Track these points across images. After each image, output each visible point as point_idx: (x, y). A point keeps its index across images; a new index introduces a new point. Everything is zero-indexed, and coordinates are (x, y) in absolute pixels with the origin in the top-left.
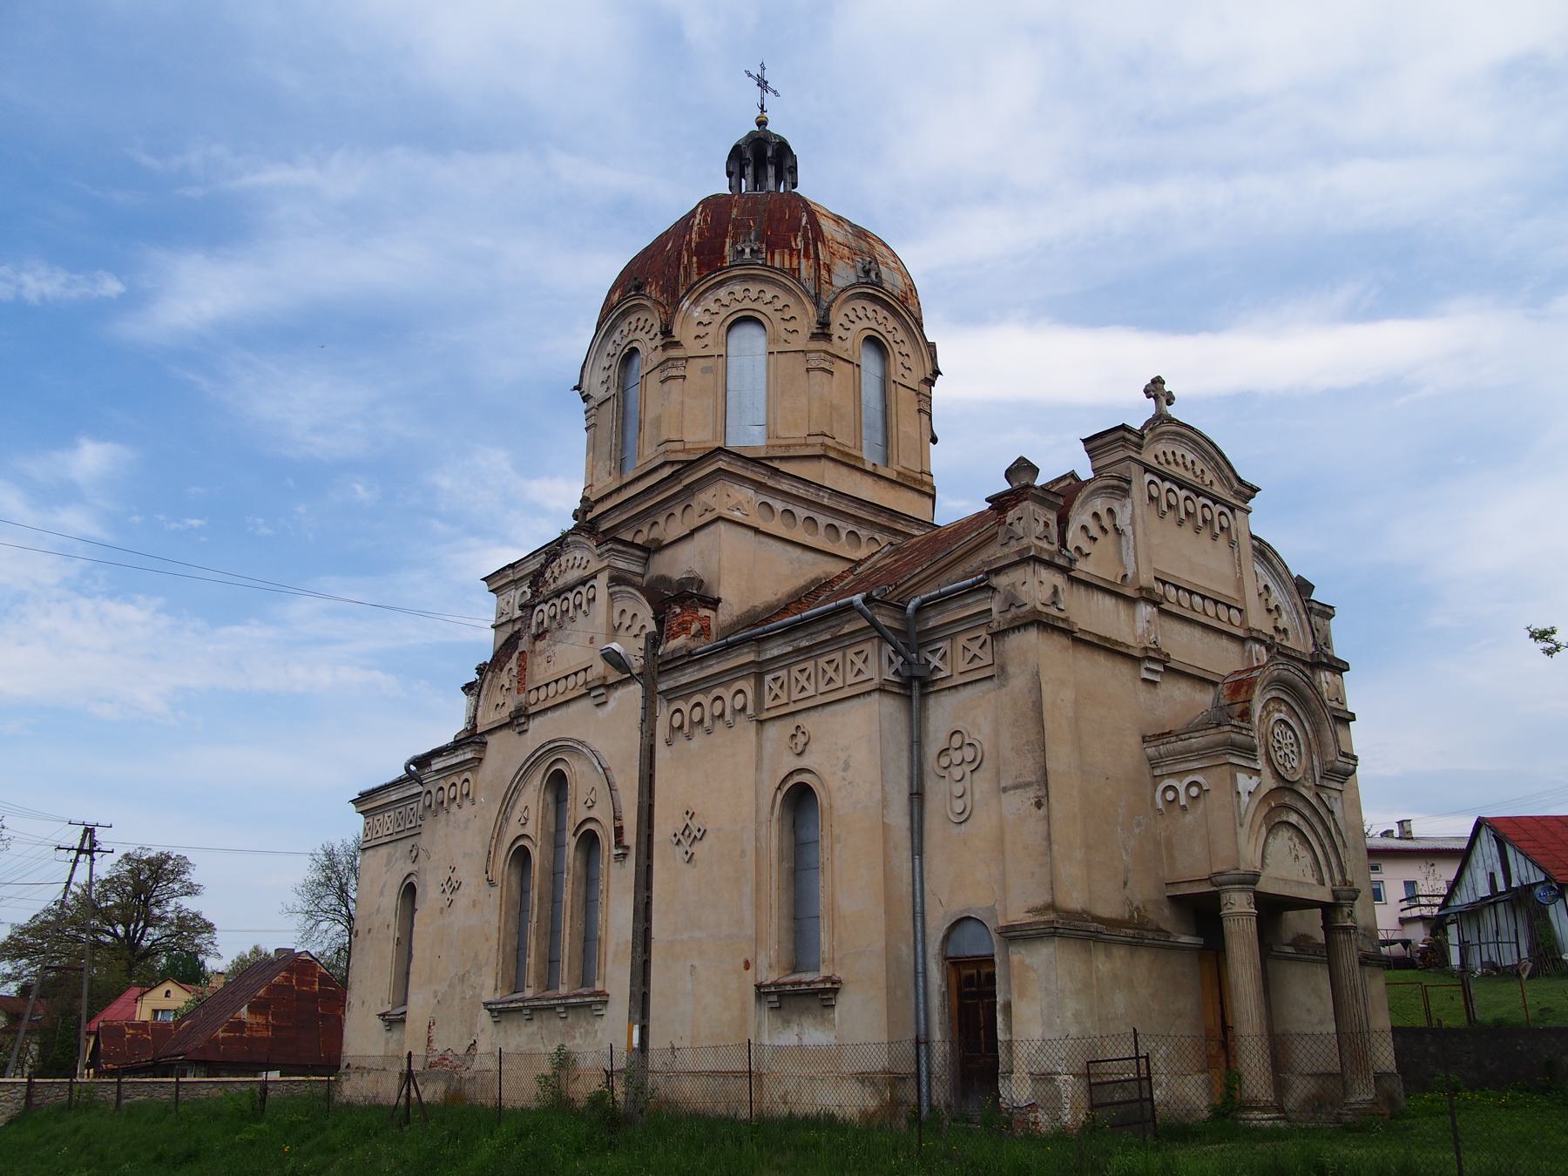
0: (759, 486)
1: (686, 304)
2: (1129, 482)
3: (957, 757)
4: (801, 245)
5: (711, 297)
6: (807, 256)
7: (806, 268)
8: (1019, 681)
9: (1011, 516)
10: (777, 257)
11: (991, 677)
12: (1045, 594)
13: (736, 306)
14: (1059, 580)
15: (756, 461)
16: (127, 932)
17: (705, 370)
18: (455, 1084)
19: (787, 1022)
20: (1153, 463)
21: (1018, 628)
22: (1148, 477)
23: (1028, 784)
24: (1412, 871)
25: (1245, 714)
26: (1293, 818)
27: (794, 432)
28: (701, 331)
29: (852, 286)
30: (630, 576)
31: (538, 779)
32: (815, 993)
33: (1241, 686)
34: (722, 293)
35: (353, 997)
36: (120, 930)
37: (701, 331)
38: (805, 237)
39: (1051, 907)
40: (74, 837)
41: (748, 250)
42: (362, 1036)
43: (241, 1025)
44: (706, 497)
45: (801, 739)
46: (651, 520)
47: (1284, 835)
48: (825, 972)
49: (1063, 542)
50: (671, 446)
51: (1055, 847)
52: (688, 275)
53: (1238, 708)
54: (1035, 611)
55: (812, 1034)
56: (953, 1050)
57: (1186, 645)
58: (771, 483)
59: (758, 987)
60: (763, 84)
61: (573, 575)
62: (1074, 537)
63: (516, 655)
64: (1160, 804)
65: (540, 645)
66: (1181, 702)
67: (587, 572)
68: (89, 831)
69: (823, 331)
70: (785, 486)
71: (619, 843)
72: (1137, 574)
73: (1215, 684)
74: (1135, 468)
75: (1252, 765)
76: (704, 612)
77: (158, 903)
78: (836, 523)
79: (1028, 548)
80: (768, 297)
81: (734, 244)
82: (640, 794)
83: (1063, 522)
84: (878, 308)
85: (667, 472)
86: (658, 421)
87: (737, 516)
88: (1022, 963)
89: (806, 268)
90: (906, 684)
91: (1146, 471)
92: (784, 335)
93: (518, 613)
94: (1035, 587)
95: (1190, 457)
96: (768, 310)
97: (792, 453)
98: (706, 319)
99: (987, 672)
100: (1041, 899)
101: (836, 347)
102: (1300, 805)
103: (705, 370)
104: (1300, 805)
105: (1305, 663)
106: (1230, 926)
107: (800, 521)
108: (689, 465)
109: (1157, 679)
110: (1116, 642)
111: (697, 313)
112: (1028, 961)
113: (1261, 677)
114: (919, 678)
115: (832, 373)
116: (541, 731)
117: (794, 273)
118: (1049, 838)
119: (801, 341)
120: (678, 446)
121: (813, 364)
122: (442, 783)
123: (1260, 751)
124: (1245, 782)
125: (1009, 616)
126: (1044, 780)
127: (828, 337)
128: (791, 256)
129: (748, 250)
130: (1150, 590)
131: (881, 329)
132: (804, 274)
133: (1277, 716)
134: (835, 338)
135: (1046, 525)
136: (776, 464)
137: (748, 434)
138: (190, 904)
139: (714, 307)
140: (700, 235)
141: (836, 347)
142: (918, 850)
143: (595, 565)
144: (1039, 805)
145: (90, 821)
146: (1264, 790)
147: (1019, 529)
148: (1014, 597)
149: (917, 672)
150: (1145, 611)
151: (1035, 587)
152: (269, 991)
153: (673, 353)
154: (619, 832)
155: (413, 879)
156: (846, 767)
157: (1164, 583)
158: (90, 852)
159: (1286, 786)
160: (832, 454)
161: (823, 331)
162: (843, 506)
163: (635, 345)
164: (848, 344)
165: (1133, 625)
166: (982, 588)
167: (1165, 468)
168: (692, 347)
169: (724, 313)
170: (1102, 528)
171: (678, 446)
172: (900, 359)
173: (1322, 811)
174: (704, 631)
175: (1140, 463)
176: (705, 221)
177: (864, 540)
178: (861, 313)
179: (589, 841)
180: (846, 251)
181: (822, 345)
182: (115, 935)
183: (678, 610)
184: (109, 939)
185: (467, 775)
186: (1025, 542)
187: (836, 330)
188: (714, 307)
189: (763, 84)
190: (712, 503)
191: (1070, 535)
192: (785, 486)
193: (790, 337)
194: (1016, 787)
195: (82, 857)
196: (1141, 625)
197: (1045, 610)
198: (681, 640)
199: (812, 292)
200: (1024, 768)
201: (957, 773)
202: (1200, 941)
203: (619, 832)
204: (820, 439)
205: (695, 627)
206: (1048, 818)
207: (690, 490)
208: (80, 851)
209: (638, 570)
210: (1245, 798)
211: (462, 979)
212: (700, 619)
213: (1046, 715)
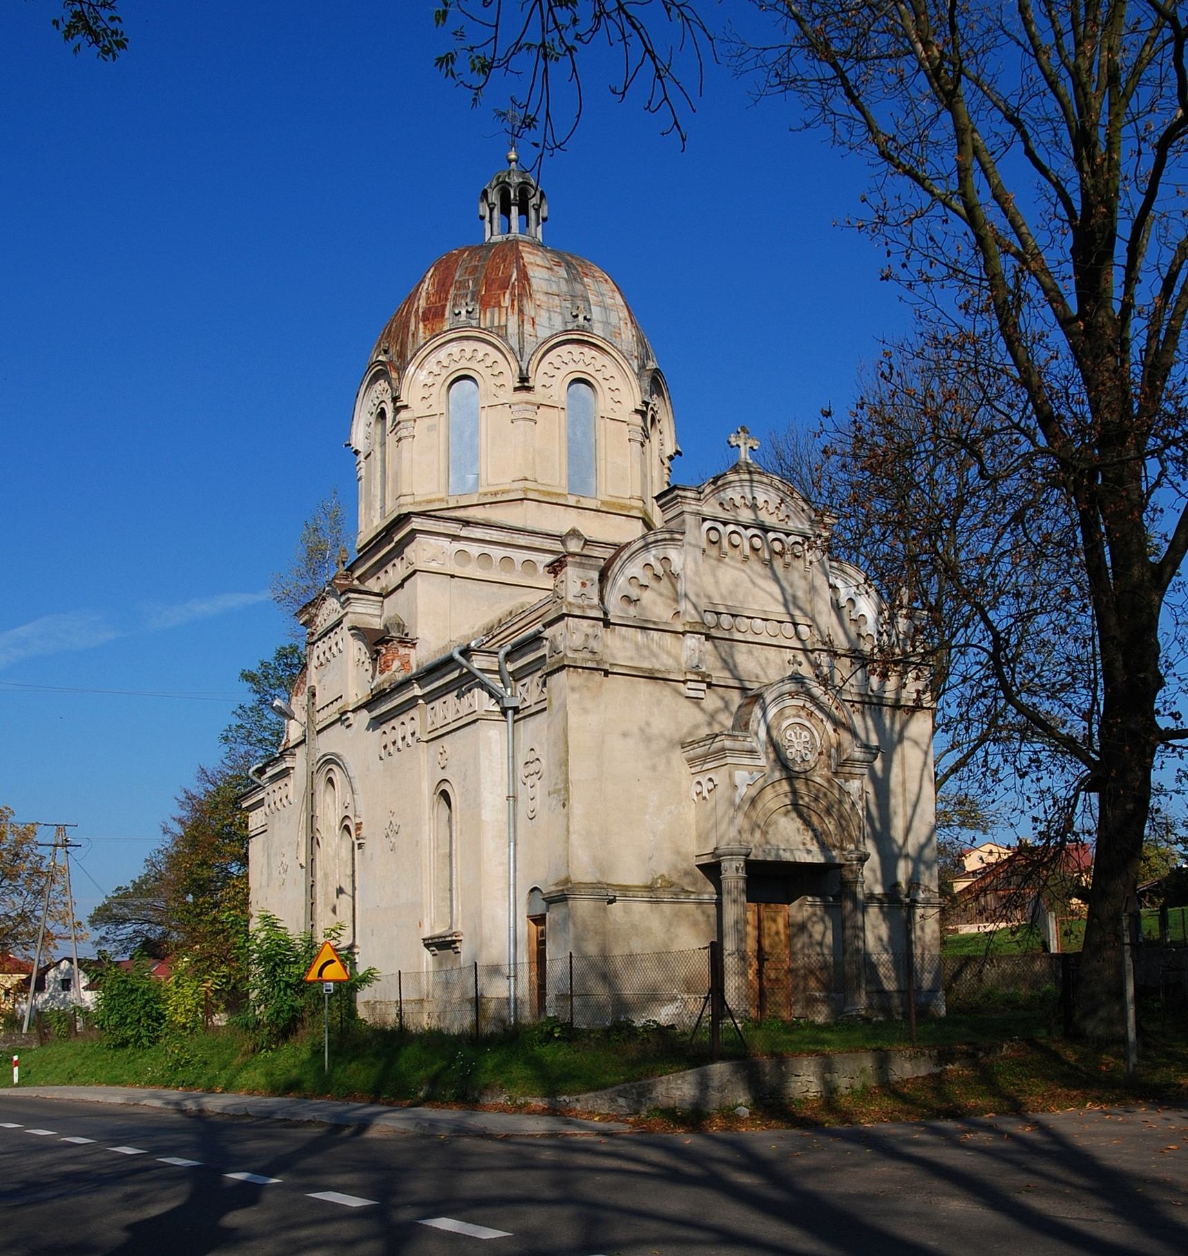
0: (455, 538)
1: (411, 369)
5: (432, 359)
10: (488, 315)
11: (545, 709)
13: (454, 367)
17: (431, 428)
34: (442, 354)
38: (512, 294)
41: (463, 312)
44: (409, 551)
56: (1098, 1100)
58: (463, 533)
61: (334, 618)
69: (524, 384)
76: (402, 651)
80: (480, 356)
84: (586, 350)
87: (434, 566)
89: (513, 327)
97: (499, 498)
98: (430, 381)
101: (537, 396)
103: (431, 428)
109: (701, 695)
111: (422, 376)
117: (502, 331)
121: (517, 415)
126: (567, 789)
129: (463, 312)
131: (581, 367)
134: (538, 388)
139: (436, 370)
150: (691, 641)
161: (524, 384)
162: (538, 542)
164: (551, 391)
169: (445, 373)
170: (658, 578)
171: (409, 499)
172: (609, 394)
174: (405, 664)
178: (566, 358)
181: (523, 395)
187: (537, 380)
188: (436, 370)
193: (500, 392)
197: (576, 655)
199: (516, 348)
206: (568, 816)
209: (377, 612)
212: (400, 657)
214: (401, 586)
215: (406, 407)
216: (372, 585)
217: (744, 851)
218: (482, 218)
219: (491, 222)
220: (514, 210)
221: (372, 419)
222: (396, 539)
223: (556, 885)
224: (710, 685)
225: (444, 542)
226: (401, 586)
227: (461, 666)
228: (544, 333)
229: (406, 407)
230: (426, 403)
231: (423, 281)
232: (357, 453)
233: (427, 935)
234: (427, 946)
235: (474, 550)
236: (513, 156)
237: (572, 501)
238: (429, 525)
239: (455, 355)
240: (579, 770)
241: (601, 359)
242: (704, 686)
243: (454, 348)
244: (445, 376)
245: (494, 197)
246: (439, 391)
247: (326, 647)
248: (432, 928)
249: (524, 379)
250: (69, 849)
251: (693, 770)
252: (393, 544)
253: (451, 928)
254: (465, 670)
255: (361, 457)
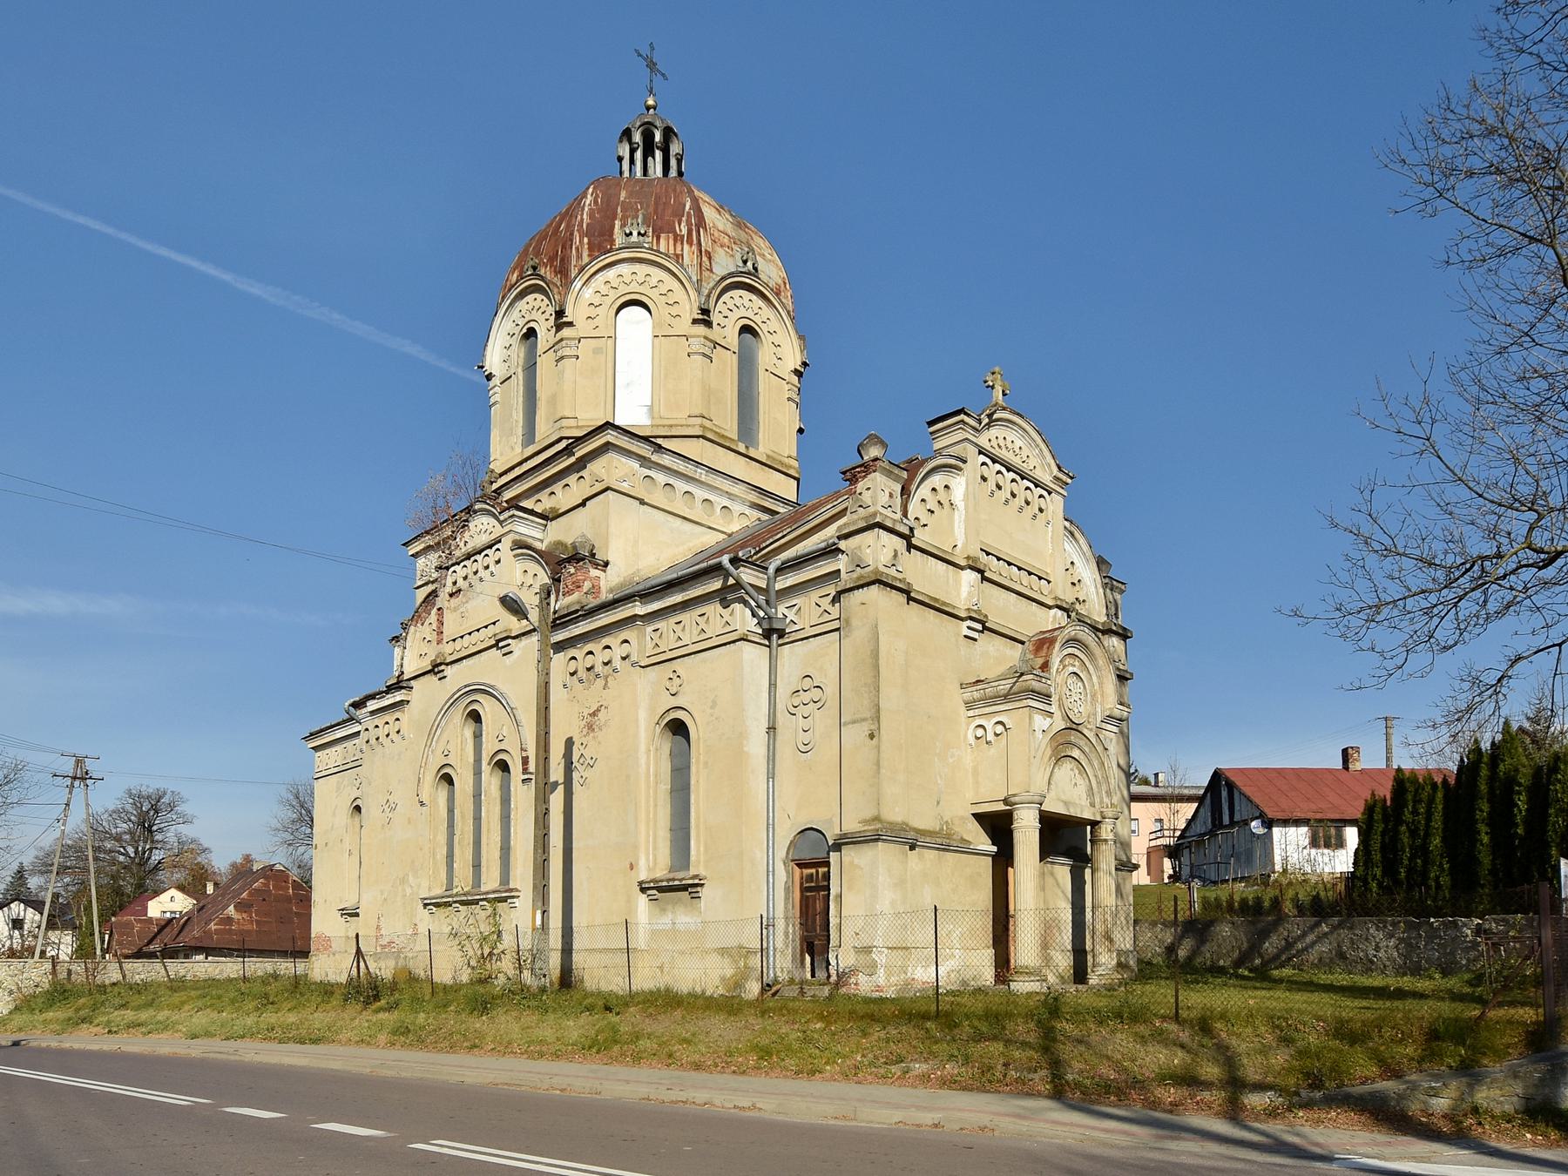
0: (644, 461)
1: (578, 284)
2: (965, 462)
3: (806, 697)
4: (684, 231)
6: (690, 243)
7: (689, 253)
8: (858, 634)
9: (860, 486)
12: (885, 557)
13: (623, 289)
14: (900, 544)
15: (646, 439)
16: (136, 852)
18: (401, 963)
19: (664, 910)
20: (987, 445)
21: (862, 586)
22: (982, 458)
23: (864, 720)
24: (1160, 809)
25: (1045, 666)
26: (1076, 753)
27: (680, 416)
28: (592, 312)
29: (731, 275)
30: (530, 541)
31: (458, 714)
32: (684, 888)
33: (1044, 643)
35: (316, 896)
36: (131, 850)
37: (592, 312)
38: (689, 224)
39: (877, 819)
40: (68, 766)
41: (635, 233)
42: (324, 922)
43: (229, 920)
44: (596, 467)
45: (677, 681)
46: (548, 490)
47: (1068, 765)
48: (693, 872)
49: (905, 515)
50: (565, 423)
51: (883, 771)
52: (579, 257)
53: (1040, 661)
54: (876, 571)
55: (681, 916)
57: (1004, 610)
58: (655, 458)
59: (640, 883)
60: (652, 65)
61: (484, 539)
62: (914, 508)
63: (434, 611)
64: (972, 740)
65: (454, 601)
66: (997, 658)
67: (493, 536)
68: (79, 762)
69: (704, 318)
70: (666, 460)
71: (525, 771)
72: (965, 545)
73: (1023, 643)
74: (973, 450)
75: (1047, 708)
76: (594, 572)
77: (160, 830)
78: (711, 498)
79: (874, 515)
80: (654, 281)
81: (623, 226)
82: (538, 724)
83: (905, 491)
85: (563, 444)
86: (553, 400)
87: (624, 487)
88: (852, 863)
90: (767, 634)
91: (980, 453)
92: (669, 319)
93: (435, 575)
94: (878, 550)
95: (1018, 443)
96: (654, 294)
99: (836, 625)
100: (868, 814)
101: (715, 333)
102: (1082, 743)
103: (597, 351)
104: (1082, 743)
105: (1095, 629)
106: (1018, 837)
107: (679, 494)
108: (579, 440)
109: (975, 635)
110: (944, 603)
111: (588, 293)
112: (856, 861)
113: (1062, 637)
114: (777, 631)
115: (711, 359)
116: (457, 677)
117: (678, 258)
118: (878, 764)
119: (684, 325)
120: (572, 423)
122: (377, 722)
123: (1054, 699)
124: (1040, 722)
125: (855, 575)
126: (877, 718)
127: (708, 324)
128: (675, 241)
129: (635, 233)
130: (976, 559)
132: (687, 260)
133: (1071, 669)
135: (891, 495)
136: (659, 441)
137: (632, 412)
138: (187, 831)
139: (604, 289)
140: (591, 215)
141: (715, 333)
142: (771, 775)
143: (499, 530)
144: (872, 736)
145: (81, 753)
146: (1056, 729)
147: (867, 497)
148: (860, 559)
149: (776, 626)
150: (970, 577)
151: (878, 550)
152: (250, 894)
153: (566, 332)
154: (525, 761)
155: (358, 802)
156: (714, 705)
157: (988, 554)
158: (83, 779)
159: (1073, 727)
160: (709, 435)
161: (704, 318)
163: (532, 324)
165: (963, 589)
166: (831, 551)
167: (997, 452)
168: (582, 327)
169: (613, 295)
171: (572, 423)
173: (1100, 749)
174: (595, 590)
175: (977, 445)
176: (596, 202)
177: (736, 515)
179: (503, 766)
180: (726, 240)
182: (126, 855)
183: (572, 570)
184: (121, 858)
185: (398, 715)
186: (871, 510)
187: (715, 318)
188: (604, 289)
189: (652, 65)
190: (603, 474)
191: (911, 508)
192: (666, 460)
193: (674, 322)
194: (854, 722)
195: (77, 783)
196: (965, 590)
198: (575, 596)
200: (856, 705)
201: (805, 710)
202: (995, 849)
203: (525, 761)
204: (699, 421)
205: (587, 585)
206: (878, 747)
207: (581, 464)
208: (75, 778)
209: (539, 535)
210: (1039, 735)
211: (403, 881)
213: (881, 662)
214: (583, 504)
215: (570, 324)
216: (544, 502)
217: (1037, 799)
218: (620, 159)
219: (632, 161)
220: (658, 154)
221: (515, 341)
222: (578, 455)
223: (865, 822)
224: (985, 628)
225: (635, 465)
226: (583, 504)
227: (727, 575)
228: (720, 271)
229: (570, 324)
230: (592, 323)
231: (585, 196)
232: (489, 377)
233: (643, 877)
234: (643, 890)
235: (661, 478)
236: (651, 102)
237: (742, 448)
238: (623, 441)
239: (624, 277)
240: (890, 699)
241: (767, 312)
242: (979, 627)
243: (625, 269)
244: (614, 299)
245: (637, 137)
246: (606, 312)
247: (470, 571)
248: (649, 870)
249: (705, 312)
250: (89, 782)
251: (971, 713)
252: (572, 460)
253: (450, 887)
254: (731, 581)
255: (496, 381)
